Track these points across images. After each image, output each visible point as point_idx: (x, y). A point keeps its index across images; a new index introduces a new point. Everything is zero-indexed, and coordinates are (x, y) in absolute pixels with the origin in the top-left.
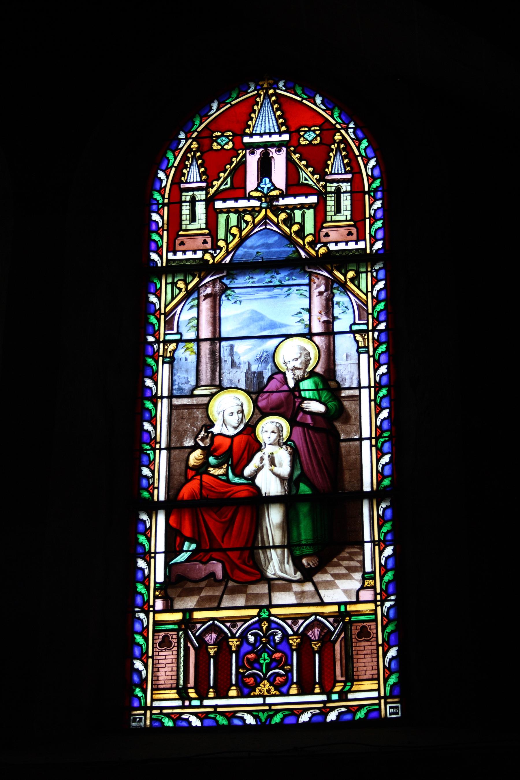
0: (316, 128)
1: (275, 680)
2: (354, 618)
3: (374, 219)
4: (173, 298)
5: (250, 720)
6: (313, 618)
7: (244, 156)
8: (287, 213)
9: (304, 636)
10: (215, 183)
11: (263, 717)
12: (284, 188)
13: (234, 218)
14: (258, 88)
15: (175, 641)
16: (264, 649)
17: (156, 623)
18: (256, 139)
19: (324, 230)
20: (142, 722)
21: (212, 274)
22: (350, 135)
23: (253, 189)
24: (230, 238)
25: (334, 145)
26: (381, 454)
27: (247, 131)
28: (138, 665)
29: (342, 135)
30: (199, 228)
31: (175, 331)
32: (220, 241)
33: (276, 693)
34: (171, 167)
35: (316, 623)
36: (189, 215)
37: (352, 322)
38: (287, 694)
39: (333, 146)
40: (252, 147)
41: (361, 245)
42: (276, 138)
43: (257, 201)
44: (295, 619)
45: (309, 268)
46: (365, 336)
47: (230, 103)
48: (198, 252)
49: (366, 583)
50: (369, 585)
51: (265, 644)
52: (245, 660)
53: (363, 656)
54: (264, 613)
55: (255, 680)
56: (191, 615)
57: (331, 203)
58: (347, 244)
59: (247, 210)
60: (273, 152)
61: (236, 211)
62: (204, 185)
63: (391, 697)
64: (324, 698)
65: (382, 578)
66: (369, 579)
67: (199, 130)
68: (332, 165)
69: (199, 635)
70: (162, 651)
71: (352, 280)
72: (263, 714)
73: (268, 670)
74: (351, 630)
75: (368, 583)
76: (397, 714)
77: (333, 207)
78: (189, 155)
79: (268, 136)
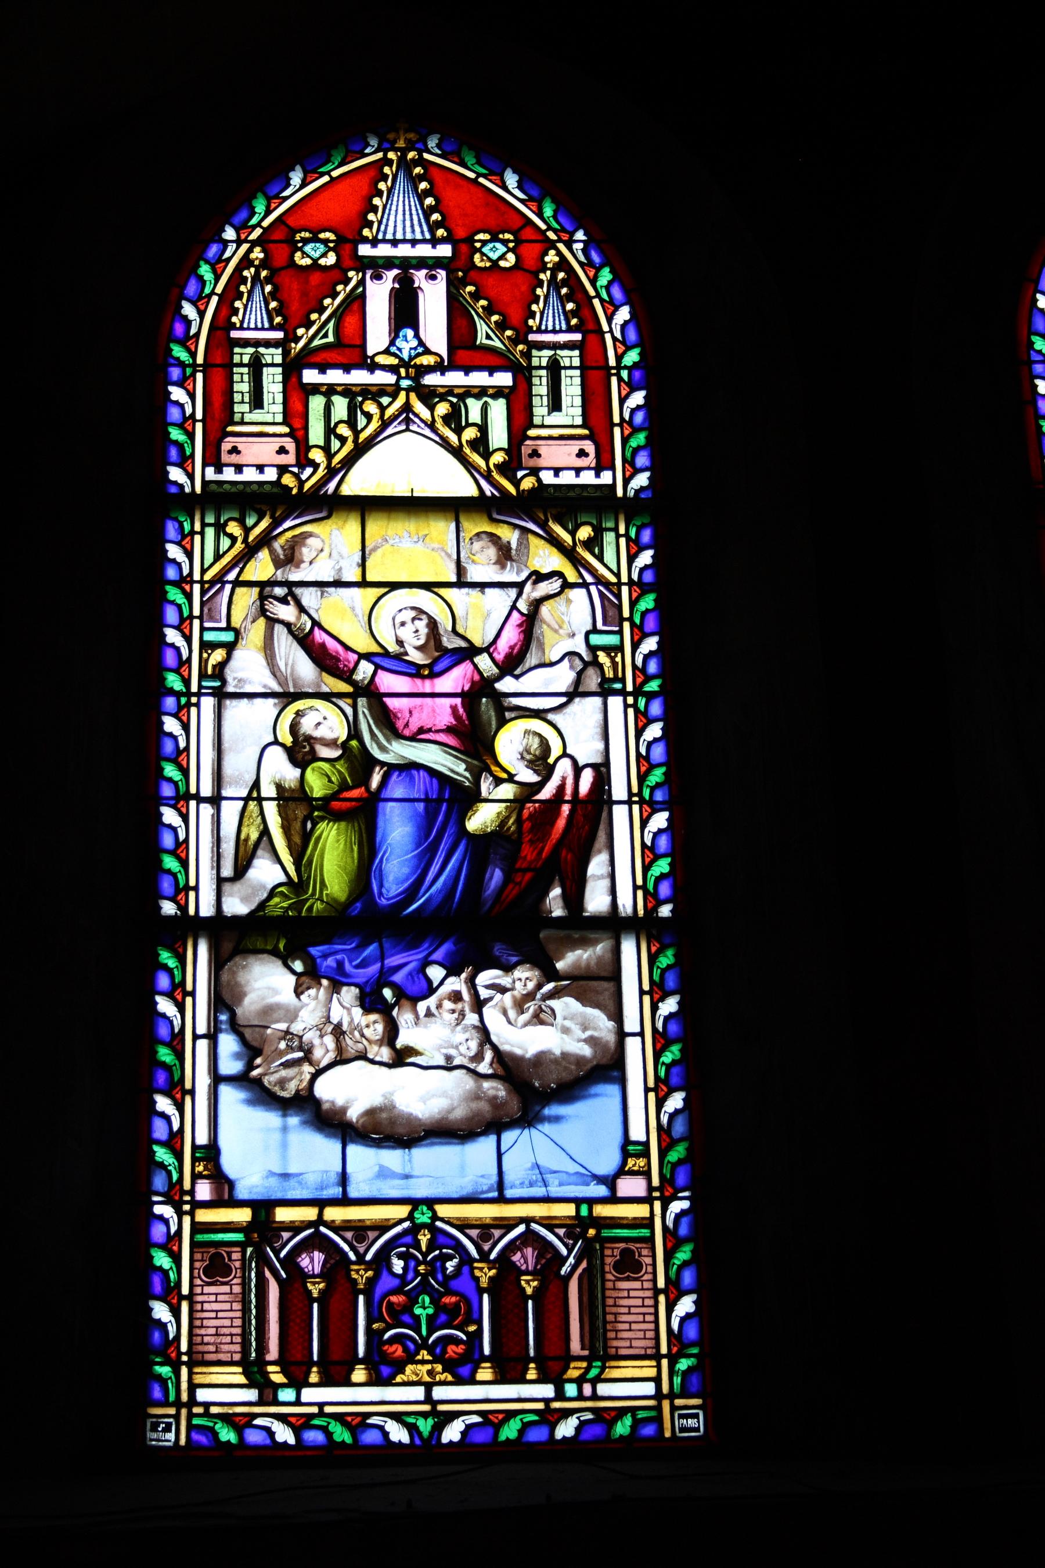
0: (508, 236)
1: (444, 1351)
2: (606, 1233)
3: (630, 427)
4: (218, 557)
5: (398, 1434)
6: (522, 1228)
7: (362, 282)
8: (452, 404)
9: (504, 1260)
10: (300, 331)
11: (425, 1426)
12: (444, 353)
13: (340, 407)
14: (386, 145)
15: (238, 1264)
16: (424, 1287)
17: (197, 1228)
18: (384, 250)
19: (528, 442)
20: (170, 1431)
21: (296, 514)
22: (576, 253)
23: (382, 349)
24: (335, 444)
25: (545, 273)
26: (644, 720)
27: (366, 232)
28: (161, 1311)
29: (559, 253)
30: (271, 421)
31: (223, 624)
32: (314, 450)
33: (446, 1377)
34: (209, 297)
35: (530, 1238)
36: (249, 392)
37: (589, 627)
38: (472, 1381)
39: (542, 276)
40: (377, 267)
41: (606, 478)
42: (424, 250)
43: (390, 374)
44: (486, 1229)
45: (498, 514)
46: (616, 656)
47: (328, 173)
48: (266, 469)
49: (631, 1162)
50: (636, 1168)
51: (425, 1277)
52: (385, 1304)
53: (626, 1310)
54: (423, 1214)
55: (406, 1349)
56: (270, 1214)
57: (541, 388)
58: (577, 475)
59: (369, 390)
60: (420, 276)
61: (347, 391)
62: (279, 335)
63: (683, 1395)
64: (547, 1391)
65: (662, 1154)
66: (637, 1156)
67: (266, 223)
68: (542, 313)
69: (285, 1256)
70: (209, 1284)
71: (588, 544)
72: (426, 1420)
73: (431, 1332)
74: (603, 1256)
75: (633, 1162)
76: (697, 1430)
77: (545, 399)
78: (246, 273)
79: (409, 245)
